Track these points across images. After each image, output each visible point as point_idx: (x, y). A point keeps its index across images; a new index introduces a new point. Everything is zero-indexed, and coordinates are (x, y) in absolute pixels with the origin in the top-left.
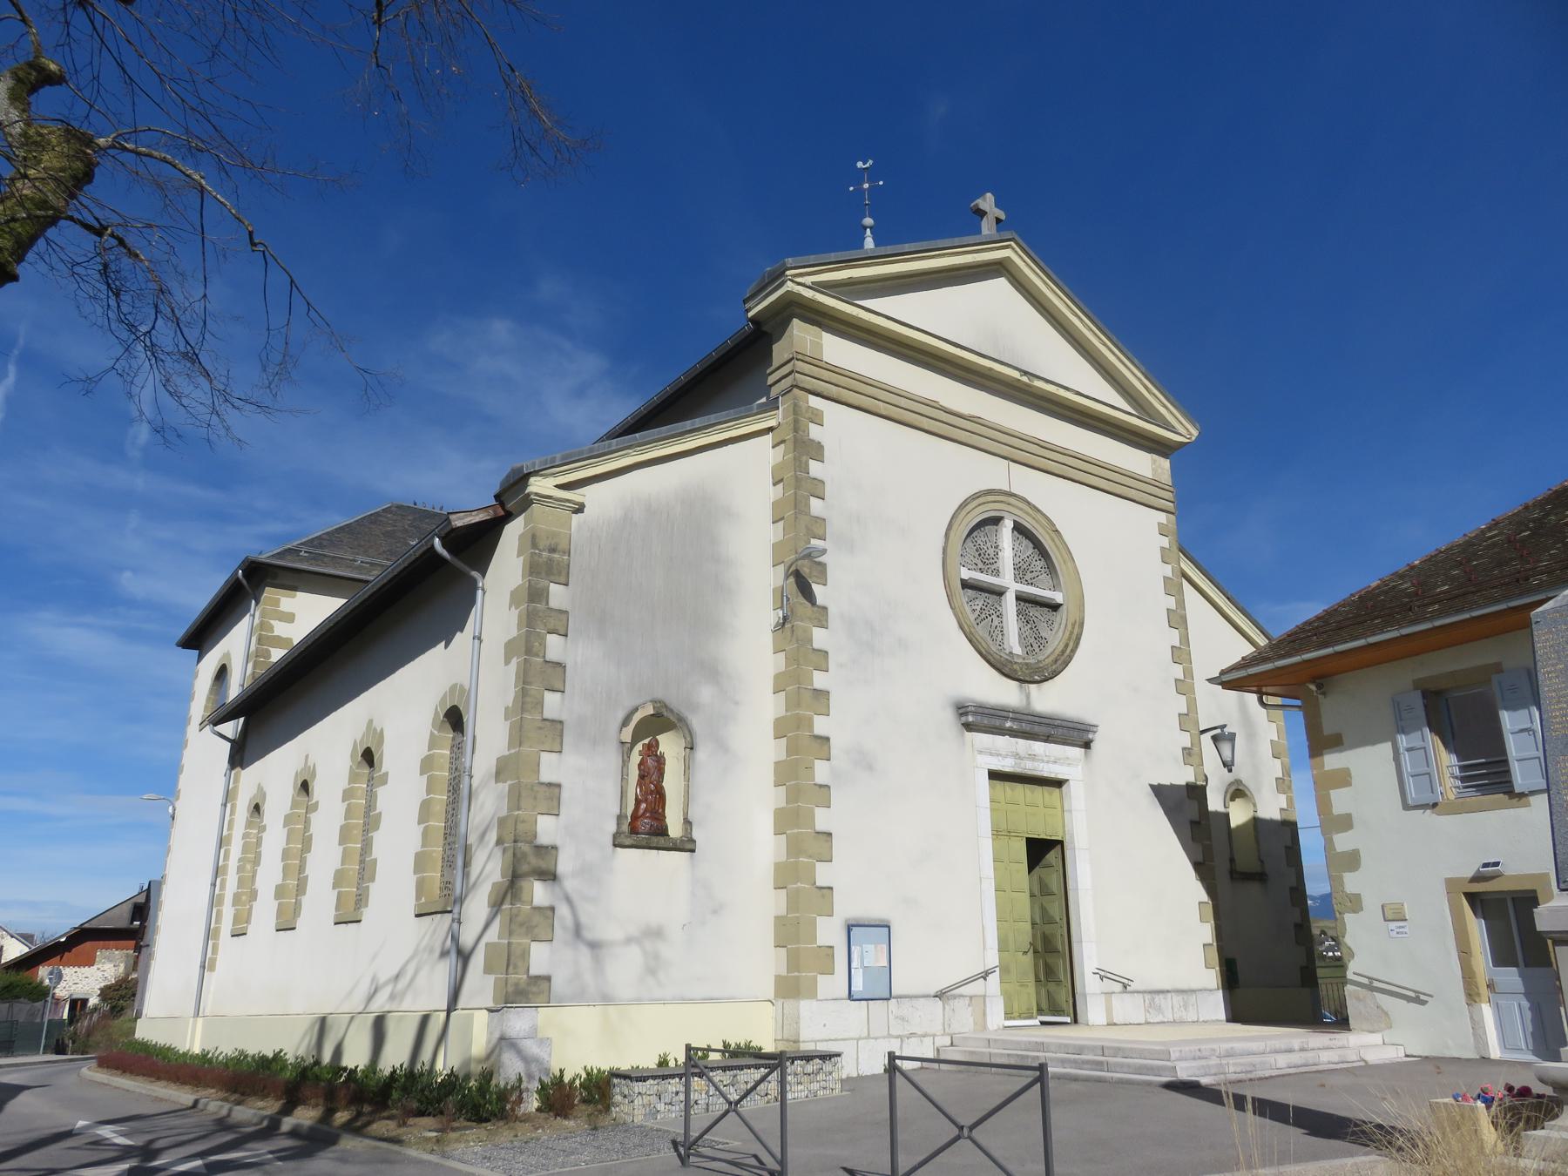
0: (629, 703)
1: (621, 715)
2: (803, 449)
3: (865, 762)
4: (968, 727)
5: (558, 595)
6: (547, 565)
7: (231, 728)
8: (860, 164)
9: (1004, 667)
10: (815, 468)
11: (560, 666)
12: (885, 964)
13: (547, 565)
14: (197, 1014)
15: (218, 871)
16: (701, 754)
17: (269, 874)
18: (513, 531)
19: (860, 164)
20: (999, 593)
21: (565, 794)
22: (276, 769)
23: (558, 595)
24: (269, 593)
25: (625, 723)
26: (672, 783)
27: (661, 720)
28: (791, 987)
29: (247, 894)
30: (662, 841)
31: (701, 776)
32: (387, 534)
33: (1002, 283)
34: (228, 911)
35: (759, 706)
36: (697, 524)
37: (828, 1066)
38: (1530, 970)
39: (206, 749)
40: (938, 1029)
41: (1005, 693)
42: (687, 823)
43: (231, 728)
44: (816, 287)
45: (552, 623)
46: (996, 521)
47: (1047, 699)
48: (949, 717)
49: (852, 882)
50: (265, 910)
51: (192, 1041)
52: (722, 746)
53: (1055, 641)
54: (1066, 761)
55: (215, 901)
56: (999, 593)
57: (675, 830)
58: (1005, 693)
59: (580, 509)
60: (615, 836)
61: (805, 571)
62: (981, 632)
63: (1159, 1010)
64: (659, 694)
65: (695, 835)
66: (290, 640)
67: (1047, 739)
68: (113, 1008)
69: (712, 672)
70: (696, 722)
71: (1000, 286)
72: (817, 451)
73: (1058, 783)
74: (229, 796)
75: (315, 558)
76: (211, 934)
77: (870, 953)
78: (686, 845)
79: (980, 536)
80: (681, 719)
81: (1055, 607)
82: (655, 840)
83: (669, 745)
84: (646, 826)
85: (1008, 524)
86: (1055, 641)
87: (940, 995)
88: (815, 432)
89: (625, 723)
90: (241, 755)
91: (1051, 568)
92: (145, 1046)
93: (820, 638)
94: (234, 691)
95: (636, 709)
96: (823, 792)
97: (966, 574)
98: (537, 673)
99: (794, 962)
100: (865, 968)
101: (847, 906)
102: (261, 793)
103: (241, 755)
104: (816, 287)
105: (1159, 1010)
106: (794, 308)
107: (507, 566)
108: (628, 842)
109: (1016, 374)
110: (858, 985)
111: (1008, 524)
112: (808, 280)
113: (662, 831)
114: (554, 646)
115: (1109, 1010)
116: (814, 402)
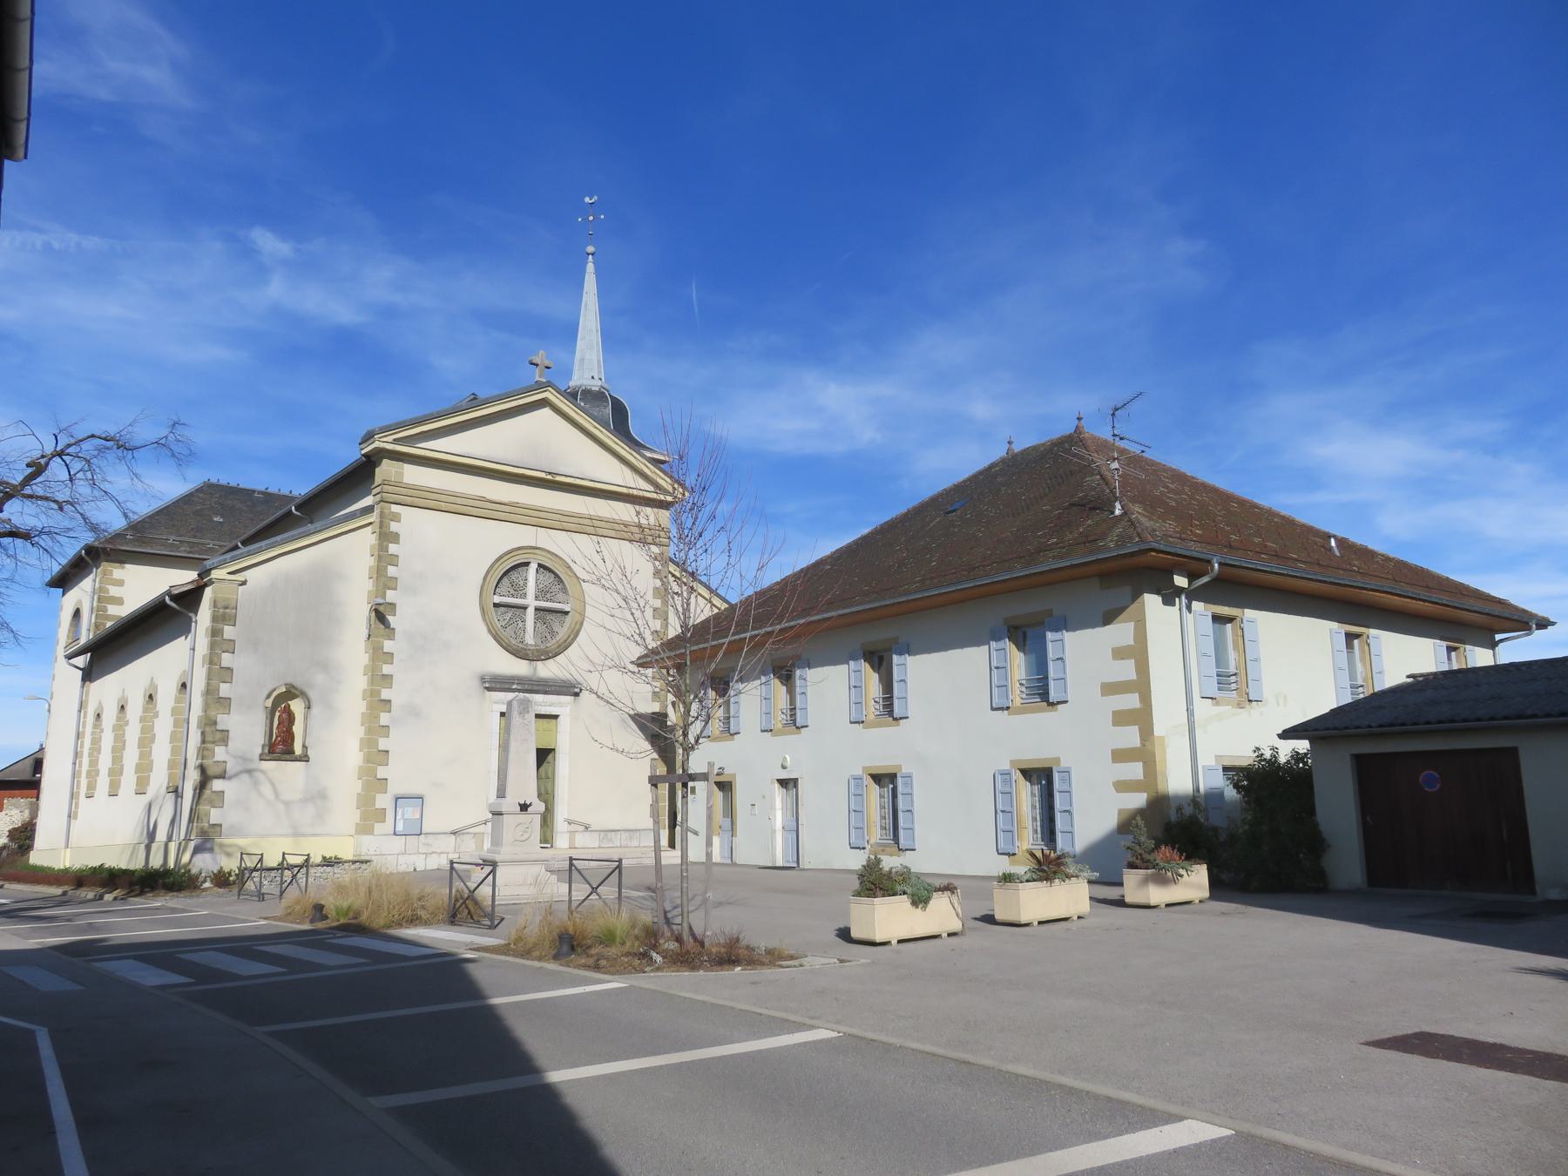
2: (386, 537)
3: (414, 712)
4: (488, 689)
5: (229, 632)
6: (224, 616)
7: (81, 661)
8: (587, 200)
9: (520, 653)
10: (393, 548)
11: (230, 670)
12: (418, 816)
13: (224, 616)
14: (67, 846)
15: (76, 755)
16: (315, 710)
17: (105, 762)
18: (208, 592)
19: (587, 200)
20: (525, 608)
21: (231, 735)
22: (110, 686)
23: (229, 632)
24: (105, 566)
26: (297, 729)
27: (291, 693)
28: (365, 828)
29: (93, 774)
32: (197, 513)
33: (546, 411)
34: (84, 782)
35: (355, 683)
36: (321, 584)
37: (364, 866)
39: (68, 675)
40: (451, 849)
41: (520, 668)
42: (305, 747)
43: (81, 661)
44: (396, 441)
45: (225, 647)
46: (527, 564)
47: (547, 670)
48: (476, 683)
49: (398, 776)
50: (103, 782)
51: (65, 860)
53: (562, 633)
54: (560, 705)
55: (75, 775)
56: (525, 608)
57: (298, 750)
58: (520, 668)
59: (244, 583)
61: (381, 609)
62: (507, 634)
63: (610, 840)
64: (290, 680)
67: (546, 693)
68: (20, 847)
69: (325, 666)
70: (312, 694)
71: (546, 412)
72: (395, 538)
73: (556, 717)
74: (82, 706)
75: (141, 540)
76: (73, 796)
77: (409, 811)
78: (305, 758)
79: (514, 575)
81: (567, 613)
83: (297, 706)
84: (281, 745)
85: (534, 566)
86: (562, 633)
87: (454, 833)
88: (394, 527)
90: (89, 675)
91: (565, 590)
92: (35, 867)
93: (388, 646)
94: (85, 638)
96: (385, 729)
97: (497, 599)
98: (218, 673)
99: (364, 817)
100: (405, 820)
101: (395, 788)
102: (100, 706)
103: (89, 675)
104: (396, 441)
105: (610, 840)
106: (381, 454)
107: (204, 617)
109: (543, 475)
110: (400, 827)
111: (534, 566)
112: (390, 439)
114: (226, 659)
115: (572, 840)
116: (395, 508)
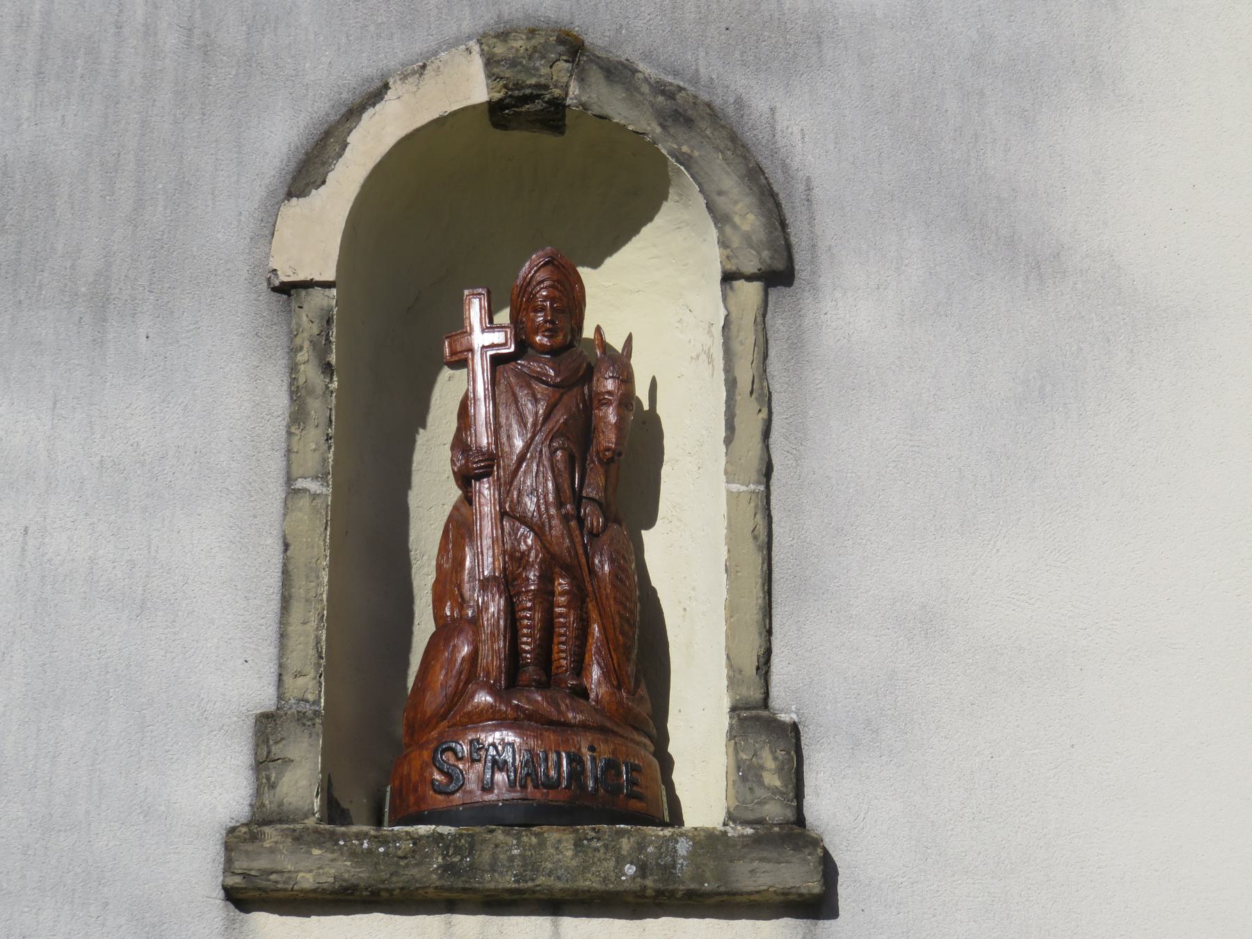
0: (327, 76)
1: (279, 136)
16: (853, 306)
25: (306, 174)
30: (619, 856)
31: (845, 444)
38: (486, 107)
42: (762, 725)
52: (1005, 242)
60: (237, 840)
65: (825, 806)
66: (595, 263)
70: (804, 126)
80: (684, 110)
82: (559, 852)
83: (655, 301)
89: (306, 174)
95: (376, 95)
108: (312, 869)
113: (630, 790)
